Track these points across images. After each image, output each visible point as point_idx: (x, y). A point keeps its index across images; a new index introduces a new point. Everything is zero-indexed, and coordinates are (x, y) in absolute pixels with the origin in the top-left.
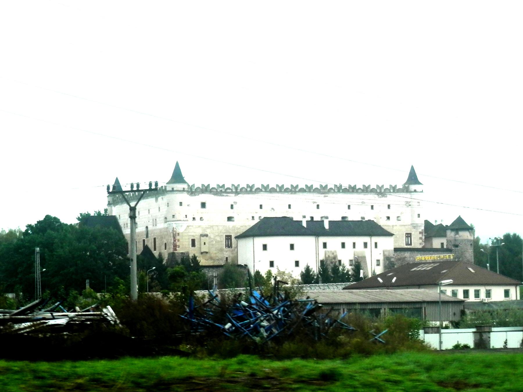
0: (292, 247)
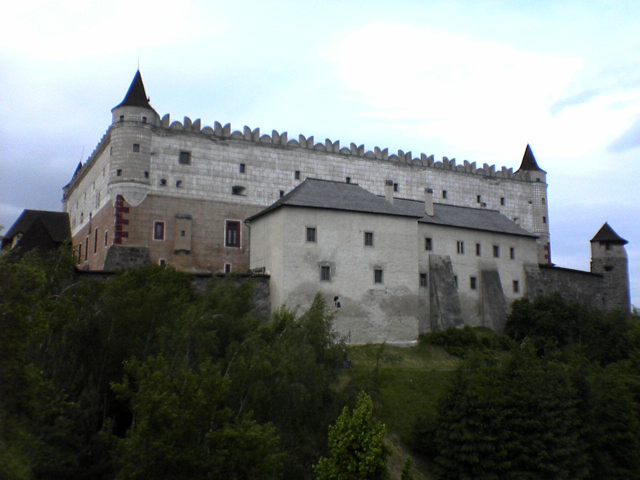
0: (369, 238)
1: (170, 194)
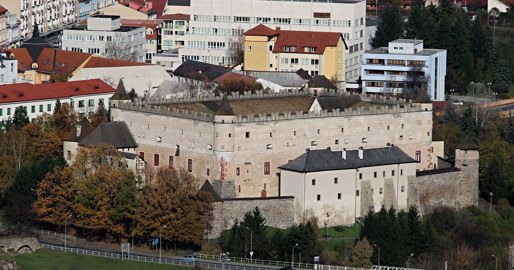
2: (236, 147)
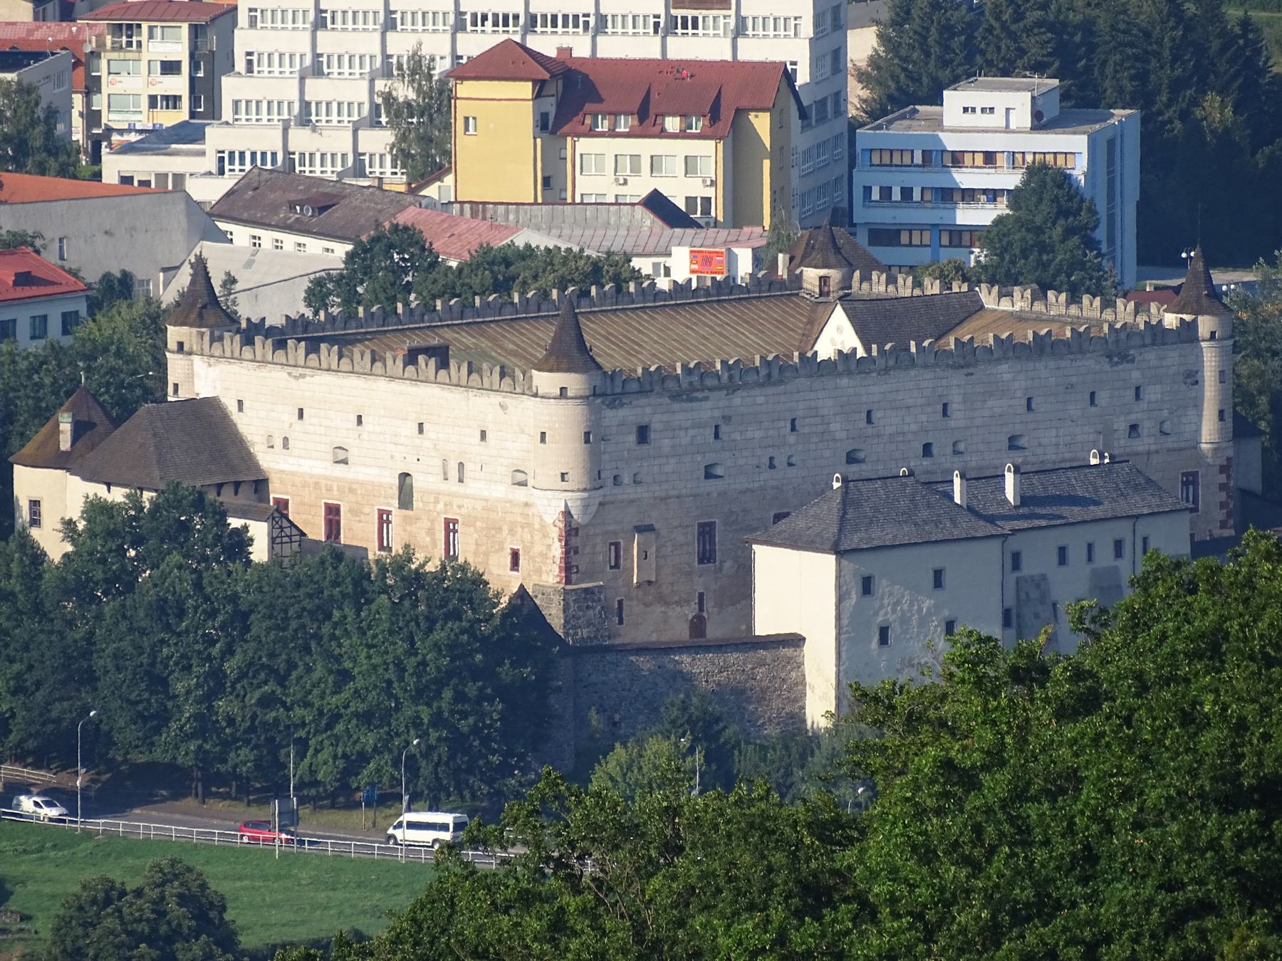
1: (625, 496)
2: (608, 475)
